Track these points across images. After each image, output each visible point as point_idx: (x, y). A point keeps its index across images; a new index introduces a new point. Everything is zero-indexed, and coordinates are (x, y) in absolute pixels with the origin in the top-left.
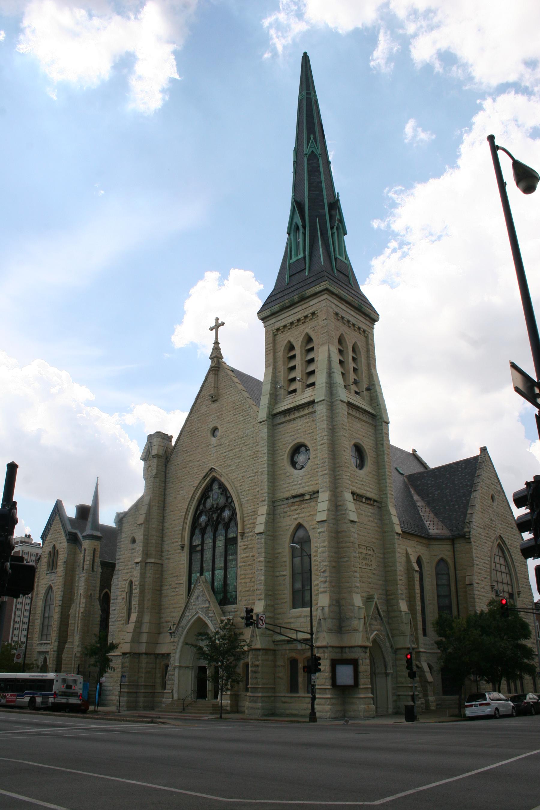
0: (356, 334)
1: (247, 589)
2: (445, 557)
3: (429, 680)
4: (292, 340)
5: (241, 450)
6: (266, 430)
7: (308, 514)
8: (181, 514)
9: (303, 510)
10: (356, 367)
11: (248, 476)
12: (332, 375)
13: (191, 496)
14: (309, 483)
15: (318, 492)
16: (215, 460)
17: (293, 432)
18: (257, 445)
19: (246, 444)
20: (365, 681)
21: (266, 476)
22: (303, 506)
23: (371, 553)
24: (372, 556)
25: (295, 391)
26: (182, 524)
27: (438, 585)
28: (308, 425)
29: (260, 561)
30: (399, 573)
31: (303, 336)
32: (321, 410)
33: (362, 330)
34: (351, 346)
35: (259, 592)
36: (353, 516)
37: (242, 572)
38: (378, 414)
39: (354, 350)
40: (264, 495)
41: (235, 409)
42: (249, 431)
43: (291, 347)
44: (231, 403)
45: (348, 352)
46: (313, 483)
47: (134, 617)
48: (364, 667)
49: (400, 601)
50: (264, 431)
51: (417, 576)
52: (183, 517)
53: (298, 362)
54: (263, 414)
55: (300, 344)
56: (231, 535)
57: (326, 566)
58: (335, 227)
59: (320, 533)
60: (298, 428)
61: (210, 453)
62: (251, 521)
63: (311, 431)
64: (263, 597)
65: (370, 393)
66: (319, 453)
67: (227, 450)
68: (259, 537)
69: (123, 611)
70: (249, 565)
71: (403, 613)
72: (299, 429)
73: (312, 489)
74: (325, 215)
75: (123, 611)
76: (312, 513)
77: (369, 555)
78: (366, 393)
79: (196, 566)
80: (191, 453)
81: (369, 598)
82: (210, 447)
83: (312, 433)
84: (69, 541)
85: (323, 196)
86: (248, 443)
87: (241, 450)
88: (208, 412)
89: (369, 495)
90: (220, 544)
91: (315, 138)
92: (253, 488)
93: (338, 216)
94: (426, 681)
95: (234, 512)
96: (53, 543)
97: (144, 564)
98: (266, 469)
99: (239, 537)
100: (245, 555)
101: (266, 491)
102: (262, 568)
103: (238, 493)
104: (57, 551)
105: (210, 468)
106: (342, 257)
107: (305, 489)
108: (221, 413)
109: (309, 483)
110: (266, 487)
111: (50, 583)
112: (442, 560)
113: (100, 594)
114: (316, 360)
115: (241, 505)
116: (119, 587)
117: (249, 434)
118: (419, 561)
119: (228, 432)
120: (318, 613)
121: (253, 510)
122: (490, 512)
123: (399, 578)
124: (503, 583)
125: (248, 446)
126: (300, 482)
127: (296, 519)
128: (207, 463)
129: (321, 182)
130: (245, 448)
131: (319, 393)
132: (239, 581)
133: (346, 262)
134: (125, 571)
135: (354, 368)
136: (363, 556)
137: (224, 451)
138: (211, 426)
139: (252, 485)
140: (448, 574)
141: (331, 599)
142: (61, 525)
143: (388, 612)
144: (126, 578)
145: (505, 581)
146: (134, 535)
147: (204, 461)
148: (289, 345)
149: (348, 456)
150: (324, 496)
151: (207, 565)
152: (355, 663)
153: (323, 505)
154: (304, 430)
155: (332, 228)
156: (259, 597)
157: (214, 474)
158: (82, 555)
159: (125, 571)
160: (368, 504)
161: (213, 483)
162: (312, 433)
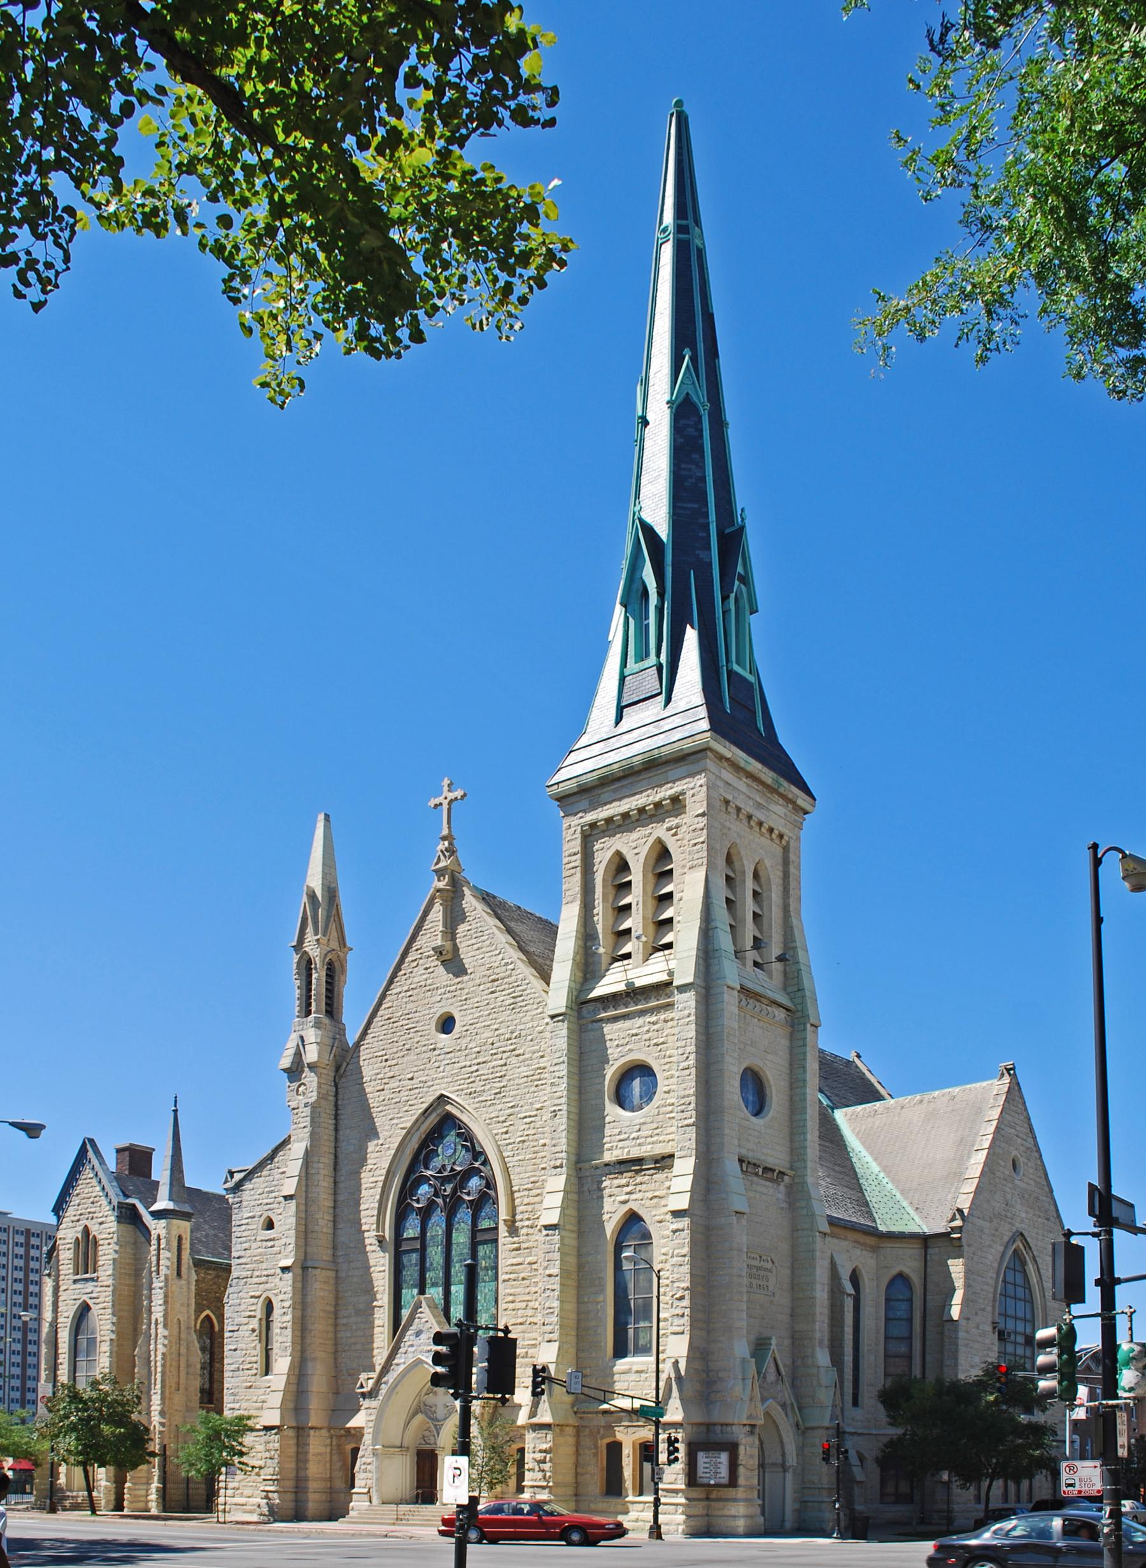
0: (765, 841)
1: (520, 1320)
2: (907, 1271)
3: (858, 1479)
4: (624, 851)
5: (505, 1065)
6: (565, 1032)
7: (649, 1195)
8: (375, 1179)
9: (639, 1188)
10: (758, 911)
11: (522, 1115)
12: (711, 932)
13: (396, 1145)
14: (654, 1139)
15: (672, 1156)
16: (450, 1080)
17: (623, 1042)
18: (542, 1057)
19: (516, 1052)
20: (747, 1476)
21: (565, 1120)
22: (639, 1179)
23: (769, 1265)
24: (770, 1271)
25: (628, 956)
26: (378, 1197)
27: (887, 1319)
28: (656, 1027)
29: (550, 1276)
30: (818, 1302)
31: (649, 844)
32: (687, 1003)
33: (776, 832)
34: (753, 868)
35: (548, 1328)
36: (739, 1203)
37: (508, 1291)
38: (799, 1007)
39: (756, 876)
40: (560, 1155)
41: (493, 981)
42: (522, 1027)
43: (621, 865)
44: (482, 968)
45: (744, 881)
46: (661, 1138)
47: (282, 1364)
48: (748, 1453)
49: (818, 1349)
50: (559, 1038)
51: (849, 1303)
52: (380, 1184)
53: (634, 898)
54: (558, 997)
55: (642, 860)
56: (485, 1224)
57: (685, 1289)
58: (733, 596)
59: (674, 1232)
60: (634, 1032)
61: (437, 1064)
62: (526, 1201)
63: (662, 1040)
64: (555, 1336)
65: (785, 966)
66: (677, 1084)
67: (475, 1061)
68: (550, 1232)
69: (255, 1352)
70: (523, 1279)
71: (822, 1370)
72: (636, 1035)
73: (660, 1150)
74: (710, 564)
75: (255, 1352)
76: (656, 1194)
77: (766, 1269)
78: (777, 967)
79: (411, 1273)
80: (394, 1062)
81: (761, 1344)
82: (436, 1052)
83: (663, 1043)
84: (120, 1219)
85: (706, 515)
86: (521, 1051)
87: (505, 1065)
88: (429, 982)
89: (771, 1162)
90: (461, 1238)
91: (694, 359)
92: (531, 1138)
93: (740, 569)
94: (852, 1480)
95: (490, 1184)
96: (83, 1222)
97: (303, 1269)
98: (564, 1107)
99: (503, 1230)
100: (515, 1261)
101: (564, 1148)
102: (554, 1287)
103: (498, 1146)
104: (94, 1237)
105: (438, 1094)
106: (744, 668)
107: (643, 1148)
108: (459, 986)
109: (654, 1139)
110: (564, 1140)
111: (85, 1297)
112: (901, 1276)
113: (196, 1319)
114: (676, 897)
115: (506, 1170)
116: (243, 1307)
117: (523, 1033)
118: (855, 1278)
119: (477, 1026)
120: (667, 1369)
121: (532, 1179)
122: (1008, 1190)
123: (818, 1310)
124: (1016, 1318)
125: (521, 1058)
126: (634, 1135)
127: (625, 1202)
128: (430, 1083)
129: (703, 479)
130: (514, 1060)
131: (681, 962)
132: (502, 1306)
133: (752, 679)
134: (255, 1280)
135: (754, 913)
136: (754, 1271)
137: (468, 1063)
138: (439, 1011)
139: (532, 1132)
140: (911, 1300)
141: (692, 1347)
142: (98, 1188)
143: (794, 1368)
144: (258, 1294)
145: (1020, 1314)
146: (270, 1214)
147: (423, 1079)
148: (618, 859)
149: (732, 1090)
150: (685, 1167)
151: (435, 1274)
152: (732, 1448)
153: (679, 1185)
154: (646, 1036)
155: (725, 598)
156: (548, 1337)
157: (448, 1107)
158: (153, 1247)
159: (255, 1280)
160: (767, 1179)
161: (441, 1124)
162: (663, 1043)
